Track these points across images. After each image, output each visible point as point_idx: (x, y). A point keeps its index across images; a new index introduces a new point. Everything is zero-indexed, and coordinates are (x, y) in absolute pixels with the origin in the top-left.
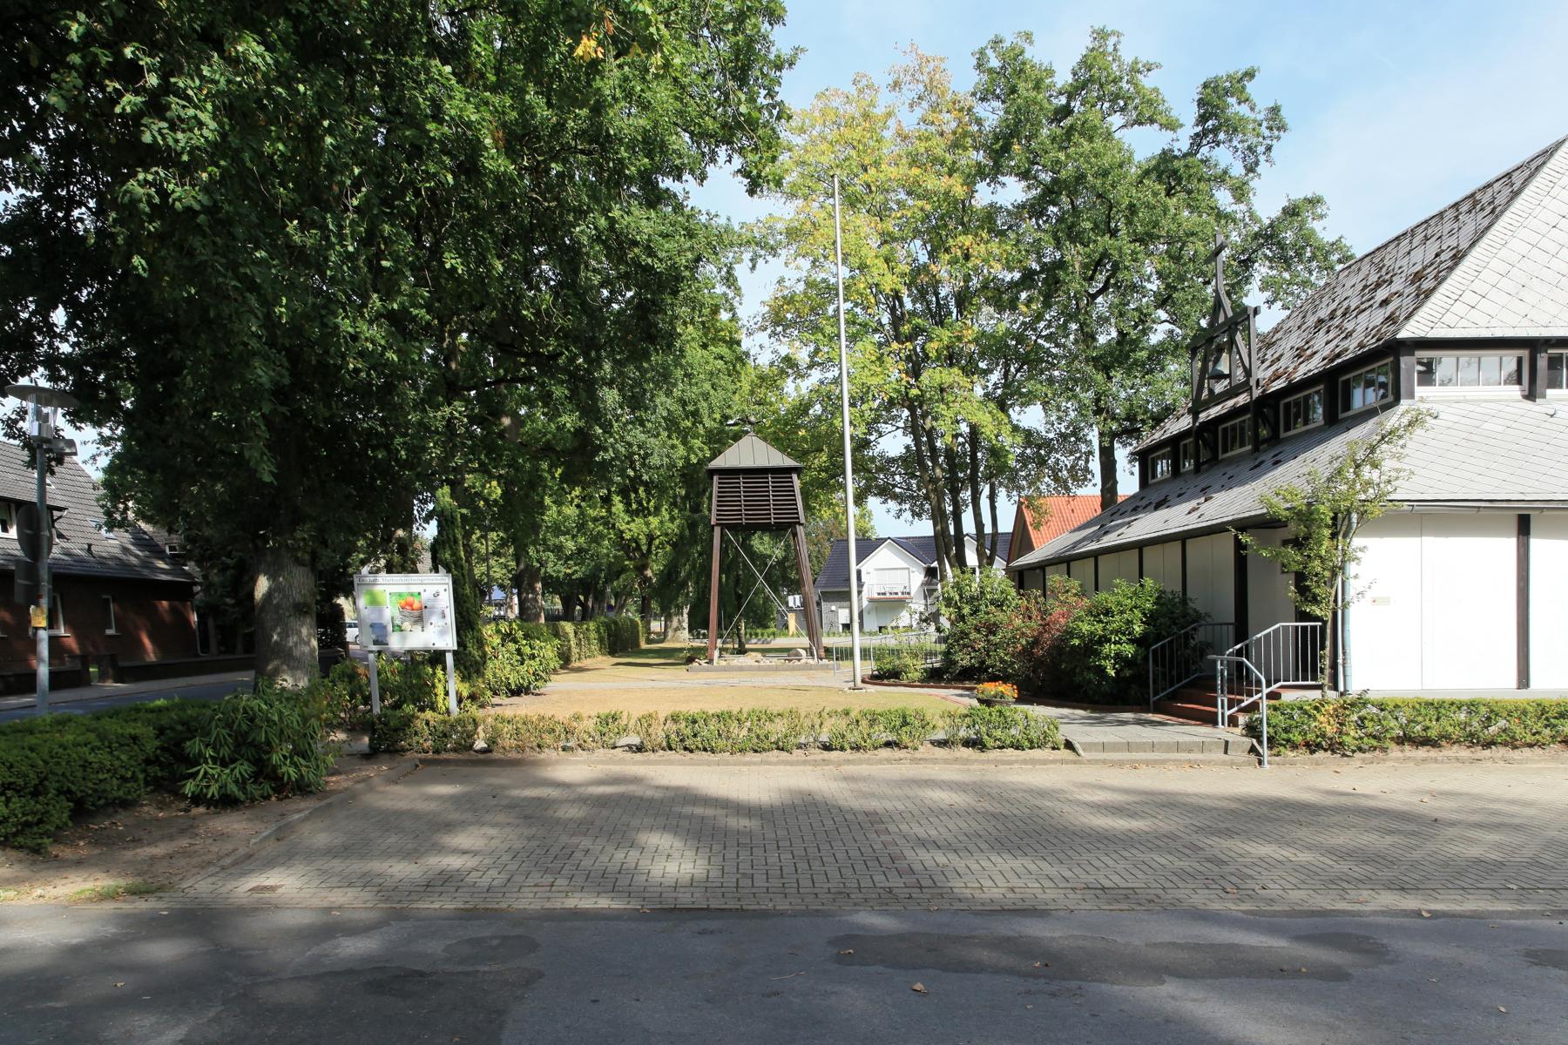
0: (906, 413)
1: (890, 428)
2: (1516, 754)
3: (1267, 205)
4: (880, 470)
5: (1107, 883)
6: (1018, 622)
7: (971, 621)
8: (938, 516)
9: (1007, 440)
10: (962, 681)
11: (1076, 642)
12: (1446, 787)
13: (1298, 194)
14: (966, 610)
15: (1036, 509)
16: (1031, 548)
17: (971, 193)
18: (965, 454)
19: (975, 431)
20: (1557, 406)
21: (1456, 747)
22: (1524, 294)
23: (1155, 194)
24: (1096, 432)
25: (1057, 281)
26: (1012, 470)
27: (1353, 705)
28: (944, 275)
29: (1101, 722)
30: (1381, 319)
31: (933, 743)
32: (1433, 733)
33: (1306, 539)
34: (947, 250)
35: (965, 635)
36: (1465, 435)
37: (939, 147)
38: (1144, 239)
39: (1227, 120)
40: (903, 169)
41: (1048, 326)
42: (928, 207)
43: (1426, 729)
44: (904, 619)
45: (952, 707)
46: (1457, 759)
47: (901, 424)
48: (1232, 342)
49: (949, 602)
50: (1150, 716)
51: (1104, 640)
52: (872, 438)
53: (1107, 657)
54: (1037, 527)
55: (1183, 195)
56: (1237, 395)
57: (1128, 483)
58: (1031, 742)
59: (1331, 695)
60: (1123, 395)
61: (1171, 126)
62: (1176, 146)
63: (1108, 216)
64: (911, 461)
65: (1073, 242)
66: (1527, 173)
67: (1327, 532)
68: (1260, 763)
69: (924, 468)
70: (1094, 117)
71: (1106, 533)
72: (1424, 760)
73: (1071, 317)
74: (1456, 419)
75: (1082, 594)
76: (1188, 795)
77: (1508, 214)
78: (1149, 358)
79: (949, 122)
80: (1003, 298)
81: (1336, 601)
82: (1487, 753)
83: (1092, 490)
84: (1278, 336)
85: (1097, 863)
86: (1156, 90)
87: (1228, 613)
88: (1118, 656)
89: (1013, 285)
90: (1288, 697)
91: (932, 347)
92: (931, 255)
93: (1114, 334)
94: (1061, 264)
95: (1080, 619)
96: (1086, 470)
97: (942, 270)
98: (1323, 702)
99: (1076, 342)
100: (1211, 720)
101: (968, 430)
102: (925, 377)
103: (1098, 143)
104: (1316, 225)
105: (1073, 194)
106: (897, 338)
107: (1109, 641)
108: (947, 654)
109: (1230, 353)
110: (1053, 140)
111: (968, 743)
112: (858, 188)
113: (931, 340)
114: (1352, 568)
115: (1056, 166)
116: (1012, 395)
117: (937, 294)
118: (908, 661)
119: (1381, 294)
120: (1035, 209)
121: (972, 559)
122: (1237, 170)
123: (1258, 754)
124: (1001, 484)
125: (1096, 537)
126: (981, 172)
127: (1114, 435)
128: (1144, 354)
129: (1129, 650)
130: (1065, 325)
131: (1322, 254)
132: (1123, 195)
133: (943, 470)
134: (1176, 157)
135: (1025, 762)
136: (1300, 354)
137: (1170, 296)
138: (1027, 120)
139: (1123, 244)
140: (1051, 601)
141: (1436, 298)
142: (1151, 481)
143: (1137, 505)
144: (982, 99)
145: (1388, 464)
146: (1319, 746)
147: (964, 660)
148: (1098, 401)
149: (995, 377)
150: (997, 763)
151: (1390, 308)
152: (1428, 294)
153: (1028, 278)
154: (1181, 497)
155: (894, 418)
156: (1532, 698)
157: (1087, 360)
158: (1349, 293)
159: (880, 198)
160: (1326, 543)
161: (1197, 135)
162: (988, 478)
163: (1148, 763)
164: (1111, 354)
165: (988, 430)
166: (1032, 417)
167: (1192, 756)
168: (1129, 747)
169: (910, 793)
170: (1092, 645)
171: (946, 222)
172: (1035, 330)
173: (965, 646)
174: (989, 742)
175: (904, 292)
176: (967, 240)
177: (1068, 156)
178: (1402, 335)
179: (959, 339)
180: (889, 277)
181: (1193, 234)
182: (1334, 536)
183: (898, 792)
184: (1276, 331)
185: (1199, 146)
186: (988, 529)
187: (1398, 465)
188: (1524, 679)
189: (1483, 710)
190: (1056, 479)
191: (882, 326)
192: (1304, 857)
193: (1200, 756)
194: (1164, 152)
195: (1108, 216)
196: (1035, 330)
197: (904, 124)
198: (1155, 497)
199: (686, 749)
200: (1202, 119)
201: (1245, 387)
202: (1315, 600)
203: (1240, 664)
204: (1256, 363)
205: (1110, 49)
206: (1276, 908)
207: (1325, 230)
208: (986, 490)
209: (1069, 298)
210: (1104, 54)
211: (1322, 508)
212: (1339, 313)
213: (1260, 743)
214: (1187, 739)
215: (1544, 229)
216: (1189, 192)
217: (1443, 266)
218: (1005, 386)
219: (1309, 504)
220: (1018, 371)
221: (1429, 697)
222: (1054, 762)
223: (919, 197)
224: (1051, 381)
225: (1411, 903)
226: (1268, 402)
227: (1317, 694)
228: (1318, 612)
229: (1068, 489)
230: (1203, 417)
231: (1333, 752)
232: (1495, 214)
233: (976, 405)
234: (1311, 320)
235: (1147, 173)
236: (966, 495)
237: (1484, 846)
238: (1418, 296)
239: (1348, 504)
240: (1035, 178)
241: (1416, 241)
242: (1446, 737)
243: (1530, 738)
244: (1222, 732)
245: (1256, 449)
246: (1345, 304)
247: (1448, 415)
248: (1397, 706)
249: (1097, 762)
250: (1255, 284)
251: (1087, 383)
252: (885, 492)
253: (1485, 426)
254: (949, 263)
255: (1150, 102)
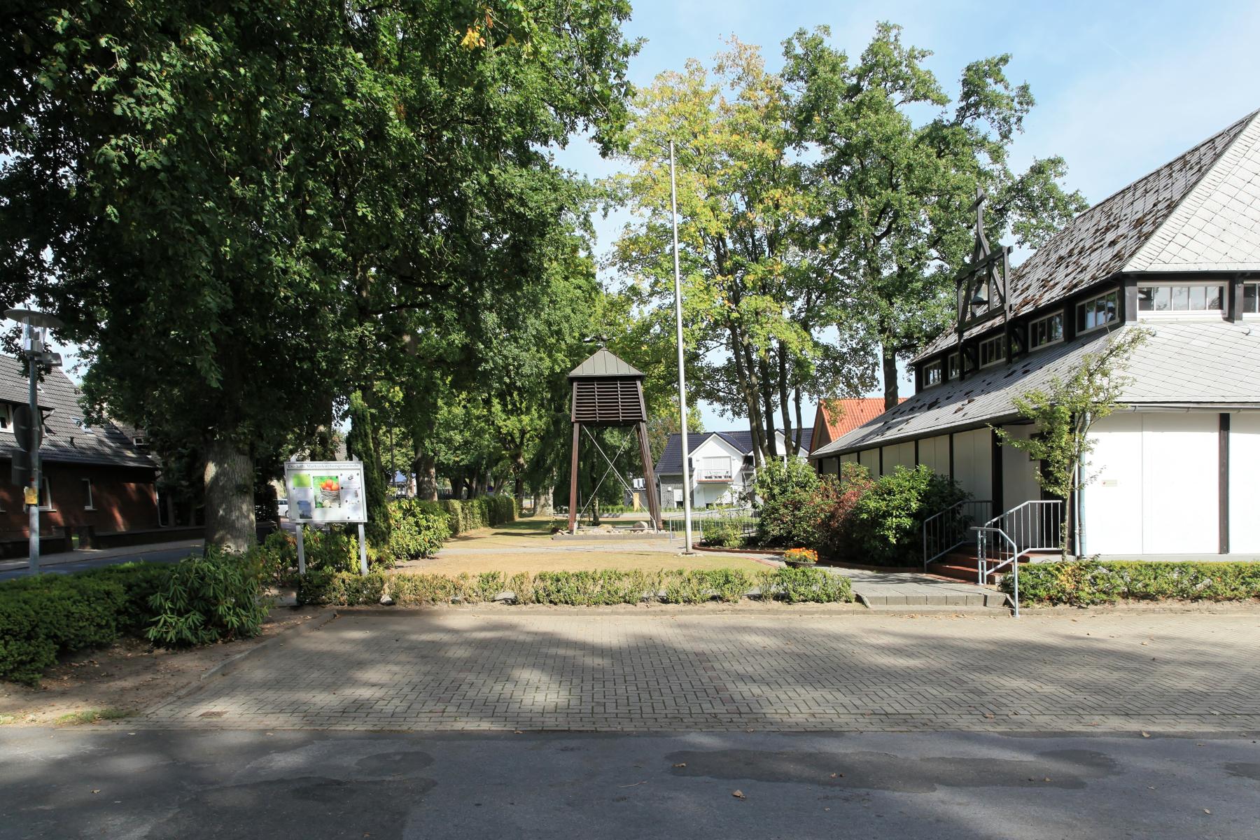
0: (728, 332)
1: (715, 344)
2: (1218, 606)
3: (1018, 165)
4: (707, 378)
5: (890, 710)
6: (818, 500)
7: (781, 499)
8: (754, 415)
9: (809, 354)
10: (773, 547)
11: (865, 516)
12: (1162, 633)
13: (1043, 156)
14: (777, 491)
15: (833, 409)
16: (828, 441)
17: (781, 155)
18: (775, 365)
19: (783, 347)
20: (1251, 326)
21: (1170, 600)
22: (1225, 236)
23: (928, 156)
24: (881, 347)
25: (850, 226)
26: (813, 377)
27: (1087, 566)
28: (758, 221)
29: (885, 580)
30: (1110, 257)
31: (749, 597)
32: (1151, 590)
33: (1049, 433)
34: (761, 201)
35: (775, 510)
36: (1177, 350)
37: (754, 118)
38: (920, 192)
39: (986, 96)
40: (726, 136)
41: (843, 262)
42: (746, 167)
43: (1146, 586)
44: (727, 497)
45: (765, 569)
46: (1171, 610)
47: (724, 341)
48: (990, 275)
49: (762, 484)
50: (924, 576)
51: (887, 514)
52: (701, 352)
53: (890, 528)
54: (833, 424)
55: (951, 157)
56: (994, 317)
57: (906, 388)
58: (829, 596)
59: (1070, 558)
60: (902, 317)
61: (941, 101)
62: (945, 117)
63: (891, 174)
64: (732, 370)
65: (862, 194)
66: (1227, 139)
67: (1066, 428)
68: (1013, 613)
69: (742, 376)
70: (879, 94)
71: (889, 428)
72: (1144, 611)
73: (861, 255)
74: (1170, 337)
75: (870, 477)
76: (954, 639)
77: (1211, 172)
78: (923, 288)
79: (763, 98)
80: (806, 240)
81: (1073, 483)
82: (1195, 605)
83: (877, 394)
84: (1027, 270)
85: (881, 694)
86: (929, 72)
87: (987, 493)
88: (898, 527)
89: (814, 229)
90: (1035, 560)
91: (749, 279)
92: (748, 205)
93: (895, 268)
94: (852, 212)
95: (868, 497)
96: (873, 378)
97: (757, 217)
98: (1063, 564)
99: (865, 275)
100: (973, 579)
101: (777, 346)
102: (743, 303)
103: (882, 115)
104: (1058, 181)
105: (862, 156)
106: (721, 272)
107: (891, 515)
108: (761, 525)
109: (988, 284)
110: (846, 113)
111: (778, 597)
112: (690, 151)
113: (748, 273)
114: (1086, 457)
115: (849, 133)
116: (813, 318)
117: (753, 236)
118: (730, 531)
119: (1110, 237)
120: (832, 168)
121: (781, 449)
122: (994, 137)
123: (1011, 606)
124: (804, 389)
125: (880, 432)
126: (788, 139)
127: (895, 350)
128: (919, 285)
129: (907, 522)
130: (856, 261)
131: (1062, 204)
132: (902, 156)
133: (758, 378)
134: (945, 126)
135: (824, 612)
136: (1045, 285)
137: (940, 238)
138: (826, 97)
139: (903, 196)
140: (844, 483)
141: (1154, 239)
142: (925, 387)
143: (914, 406)
144: (789, 80)
145: (1115, 373)
146: (1060, 600)
147: (774, 530)
148: (882, 322)
149: (800, 303)
150: (801, 613)
151: (1117, 248)
152: (1148, 236)
153: (826, 223)
154: (949, 399)
155: (718, 336)
156: (1231, 561)
157: (874, 290)
158: (1084, 236)
159: (707, 159)
160: (1066, 437)
161: (962, 108)
162: (794, 384)
163: (922, 613)
164: (893, 284)
165: (794, 346)
166: (829, 335)
167: (957, 608)
168: (907, 600)
169: (731, 637)
170: (878, 519)
171: (760, 178)
172: (831, 265)
173: (775, 519)
174: (795, 597)
175: (727, 235)
176: (777, 193)
177: (858, 126)
178: (1127, 269)
179: (771, 272)
180: (714, 223)
181: (958, 188)
182: (1072, 431)
183: (721, 636)
184: (1025, 266)
185: (964, 117)
186: (794, 426)
187: (1123, 374)
188: (1224, 546)
189: (1192, 571)
190: (849, 385)
191: (709, 262)
192: (1048, 689)
193: (964, 608)
194: (935, 122)
195: (891, 174)
196: (831, 265)
197: (726, 100)
198: (928, 400)
199: (551, 602)
200: (966, 96)
201: (1001, 311)
202: (1057, 482)
203: (997, 534)
204: (1009, 292)
205: (892, 39)
206: (1025, 730)
207: (1065, 185)
208: (792, 394)
209: (859, 239)
210: (887, 43)
211: (1062, 409)
212: (1076, 251)
213: (1013, 597)
214: (954, 594)
215: (1241, 184)
216: (956, 154)
217: (1160, 214)
218: (808, 310)
219: (1052, 405)
220: (818, 298)
221: (1148, 560)
222: (847, 612)
223: (739, 159)
224: (844, 306)
225: (1134, 726)
226: (1019, 323)
227: (1058, 558)
228: (1059, 492)
229: (858, 393)
230: (966, 335)
231: (1072, 604)
232: (1202, 172)
233: (784, 325)
234: (1054, 257)
235: (921, 139)
236: (776, 398)
237: (1192, 680)
238: (1139, 238)
239: (1083, 405)
240: (832, 143)
241: (1138, 194)
242: (1162, 592)
243: (1229, 593)
244: (982, 588)
245: (1009, 361)
246: (1081, 244)
247: (1163, 334)
248: (1122, 568)
249: (881, 612)
250: (1009, 228)
251: (873, 307)
252: (711, 396)
253: (1194, 342)
254: (763, 211)
255: (924, 82)
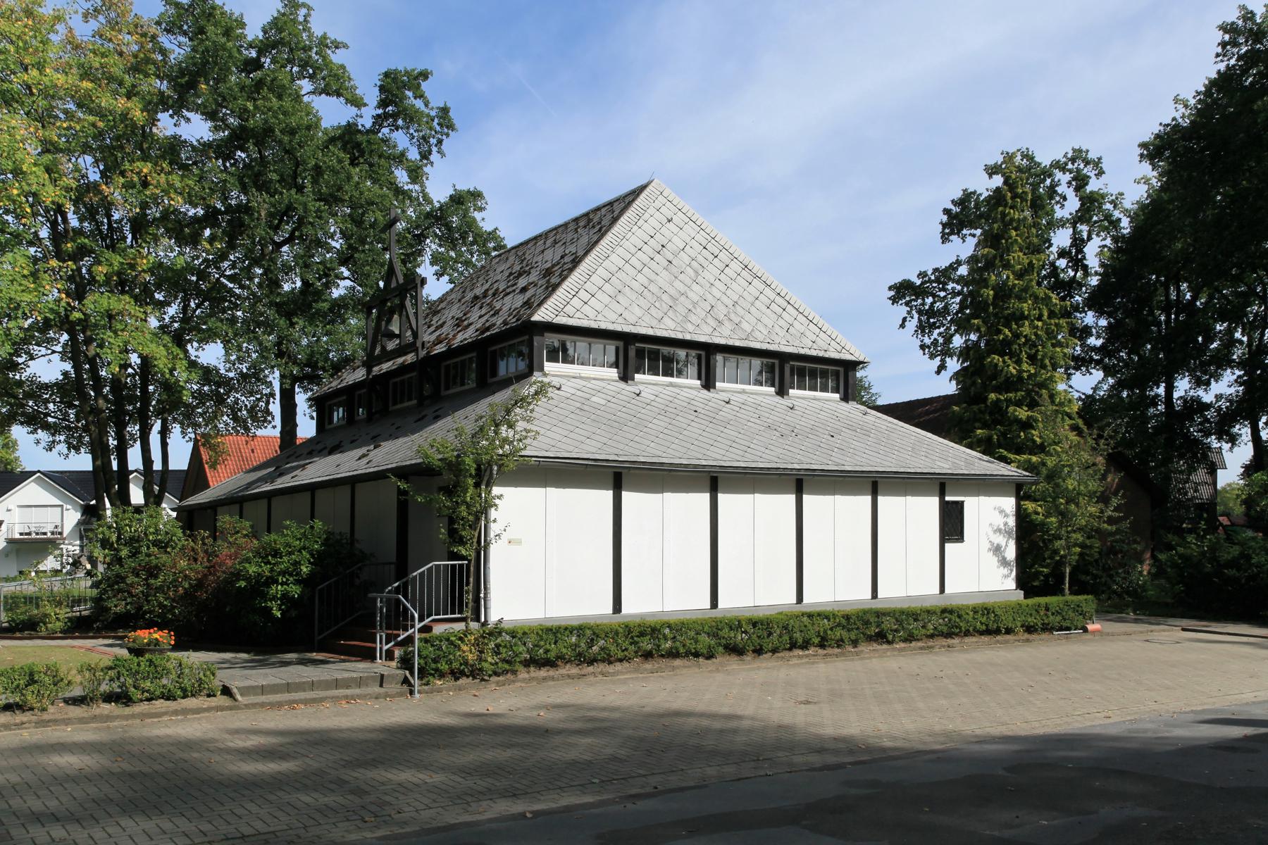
0: (65, 337)
1: (43, 351)
2: (611, 669)
3: (438, 190)
4: (28, 395)
5: (246, 830)
6: (183, 563)
7: (131, 563)
8: (99, 451)
9: (181, 375)
10: (115, 629)
11: (243, 584)
12: (559, 701)
13: (463, 186)
14: (124, 552)
15: (213, 448)
16: (207, 486)
17: (153, 121)
18: (135, 386)
19: (146, 361)
20: (641, 387)
21: (568, 666)
22: (620, 298)
23: (340, 161)
24: (277, 374)
25: (242, 224)
26: (187, 406)
27: (491, 634)
28: (117, 196)
29: (263, 664)
30: (519, 304)
31: (66, 701)
32: (552, 655)
33: (454, 487)
34: (123, 174)
35: (120, 578)
36: (578, 405)
37: (117, 67)
38: (331, 199)
39: (405, 109)
40: (73, 79)
41: (233, 266)
42: (101, 124)
43: (547, 651)
44: (50, 563)
45: (94, 659)
46: (569, 676)
47: (58, 348)
48: (402, 307)
49: (105, 543)
50: (314, 655)
51: (272, 581)
52: (20, 360)
53: (274, 598)
54: (213, 466)
55: (366, 167)
56: (405, 354)
57: (306, 428)
58: (184, 690)
59: (474, 625)
60: (305, 342)
61: (357, 102)
63: (295, 172)
64: (67, 389)
65: (259, 189)
66: (623, 205)
67: (471, 481)
68: (412, 693)
69: (84, 397)
70: (283, 77)
71: (281, 475)
72: (544, 679)
73: (256, 262)
74: (573, 391)
75: (255, 534)
76: (341, 731)
77: (610, 234)
78: (331, 310)
79: (130, 43)
80: (185, 232)
81: (479, 542)
82: (591, 669)
83: (272, 431)
84: (442, 305)
85: (239, 811)
86: (343, 67)
87: (392, 554)
88: (285, 596)
89: (195, 219)
90: (438, 629)
91: (101, 270)
92: (103, 174)
93: (299, 284)
94: (245, 209)
95: (248, 560)
96: (268, 412)
97: (115, 192)
98: (467, 632)
99: (260, 286)
100: (369, 655)
101: (139, 361)
102: (89, 300)
103: (287, 103)
104: (478, 216)
105: (260, 144)
106: (59, 255)
107: (276, 582)
108: (97, 601)
109: (400, 316)
110: (242, 88)
111: (109, 698)
112: (16, 87)
113: (99, 263)
114: (493, 513)
115: (243, 114)
116: (190, 331)
117: (109, 216)
118: (49, 609)
119: (522, 282)
120: (222, 150)
121: (137, 495)
122: (413, 155)
123: (410, 685)
124: (175, 420)
125: (270, 478)
126: (163, 102)
127: (295, 379)
128: (326, 305)
129: (295, 590)
130: (249, 268)
131: (485, 240)
132: (310, 155)
133: (107, 401)
134: (359, 131)
135: (176, 713)
136: (460, 324)
137: (352, 256)
138: (216, 63)
139: (308, 200)
140: (219, 542)
141: (560, 292)
142: (328, 427)
143: (317, 448)
144: (168, 31)
145: (521, 425)
146: (462, 674)
147: (117, 606)
148: (279, 344)
149: (172, 310)
150: (143, 716)
151: (528, 294)
152: (555, 287)
153: (211, 217)
154: (354, 444)
155: (50, 341)
156: (622, 621)
157: (272, 304)
158: (499, 277)
159: (42, 103)
160: (471, 491)
161: (379, 116)
162: (160, 413)
163: (306, 702)
164: (295, 302)
165: (162, 363)
166: (211, 354)
167: (349, 692)
168: (288, 687)
169: (29, 760)
170: (259, 587)
171: (120, 144)
172: (218, 268)
173: (120, 591)
174: (136, 695)
175: (70, 208)
176: (146, 168)
177: (256, 107)
178: (536, 318)
179: (132, 267)
180: (50, 188)
181: (373, 203)
182: (477, 485)
183: (14, 762)
184: (441, 300)
185: (381, 126)
186: (157, 466)
187: (529, 427)
188: (714, 603)
189: (588, 632)
190: (235, 418)
191: (40, 240)
192: (438, 778)
193: (357, 691)
194: (349, 124)
195: (295, 172)
196: (218, 268)
197: (77, 33)
198: (330, 442)
200: (383, 104)
201: (411, 348)
202: (461, 542)
203: (398, 601)
204: (422, 329)
205: (301, 19)
206: (408, 830)
207: (486, 220)
208: (157, 426)
209: (253, 242)
210: (294, 21)
211: (467, 460)
212: (490, 292)
213: (412, 674)
214: (346, 675)
215: (633, 250)
216: (371, 165)
217: (566, 267)
218: (182, 321)
219: (458, 456)
220: (198, 306)
221: (549, 624)
222: (209, 709)
223: (91, 112)
224: (233, 320)
225: (519, 807)
226: (430, 364)
227: (461, 626)
228: (463, 552)
229: (247, 429)
231: (474, 678)
232: (602, 233)
233: (148, 336)
234: (469, 296)
235: (332, 140)
236: (134, 429)
237: (583, 748)
238: (547, 288)
239: (488, 457)
240: (223, 120)
241: (549, 242)
242: (561, 657)
243: (620, 655)
244: (380, 666)
245: (420, 404)
246: (495, 286)
247: (568, 387)
248: (525, 633)
249: (254, 705)
250: (427, 258)
251: (269, 326)
252: (35, 421)
253: (594, 399)
254: (124, 186)
255: (337, 77)
